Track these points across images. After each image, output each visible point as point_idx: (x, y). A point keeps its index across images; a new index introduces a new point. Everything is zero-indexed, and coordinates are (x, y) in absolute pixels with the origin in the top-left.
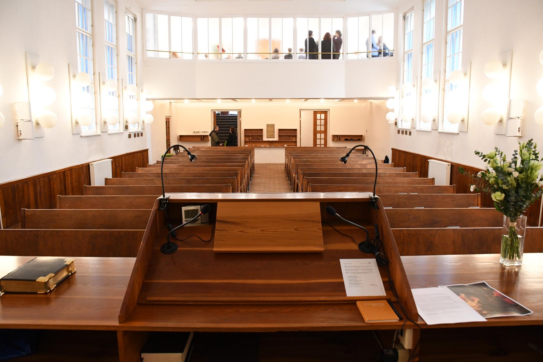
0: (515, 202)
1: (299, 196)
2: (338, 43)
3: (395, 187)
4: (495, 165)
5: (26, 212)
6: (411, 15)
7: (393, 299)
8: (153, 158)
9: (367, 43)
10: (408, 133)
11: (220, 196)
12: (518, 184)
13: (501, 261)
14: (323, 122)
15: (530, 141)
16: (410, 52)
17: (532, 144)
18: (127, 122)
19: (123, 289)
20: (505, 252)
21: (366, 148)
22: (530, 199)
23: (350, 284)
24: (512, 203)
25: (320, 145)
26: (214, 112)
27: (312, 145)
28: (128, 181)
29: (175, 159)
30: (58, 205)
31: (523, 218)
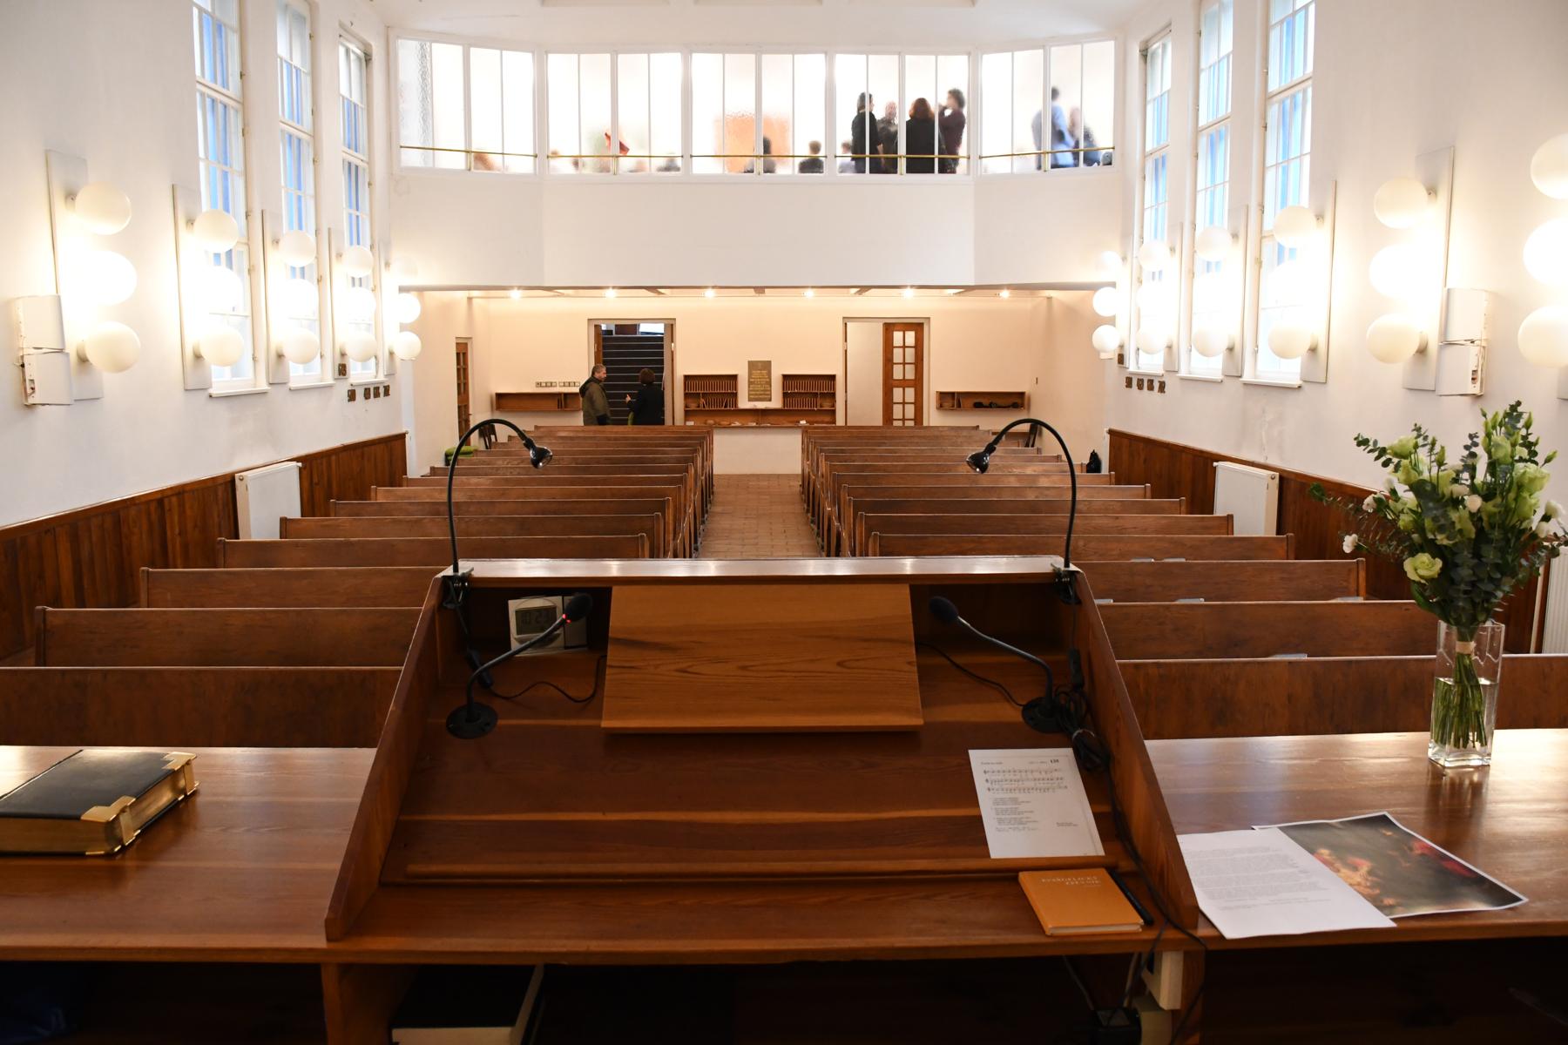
0: (1473, 584)
1: (842, 567)
2: (953, 127)
3: (1119, 540)
4: (1414, 477)
5: (49, 618)
6: (1164, 46)
7: (1126, 865)
8: (419, 461)
9: (1037, 130)
10: (1156, 385)
11: (613, 568)
12: (1480, 531)
13: (1430, 753)
14: (910, 354)
15: (1514, 408)
16: (1163, 152)
17: (1520, 414)
18: (343, 355)
19: (341, 840)
20: (1443, 725)
21: (1037, 426)
22: (1514, 574)
23: (1000, 821)
24: (1463, 587)
25: (904, 420)
26: (597, 327)
27: (880, 423)
28: (346, 525)
29: (484, 463)
30: (143, 596)
31: (1493, 627)
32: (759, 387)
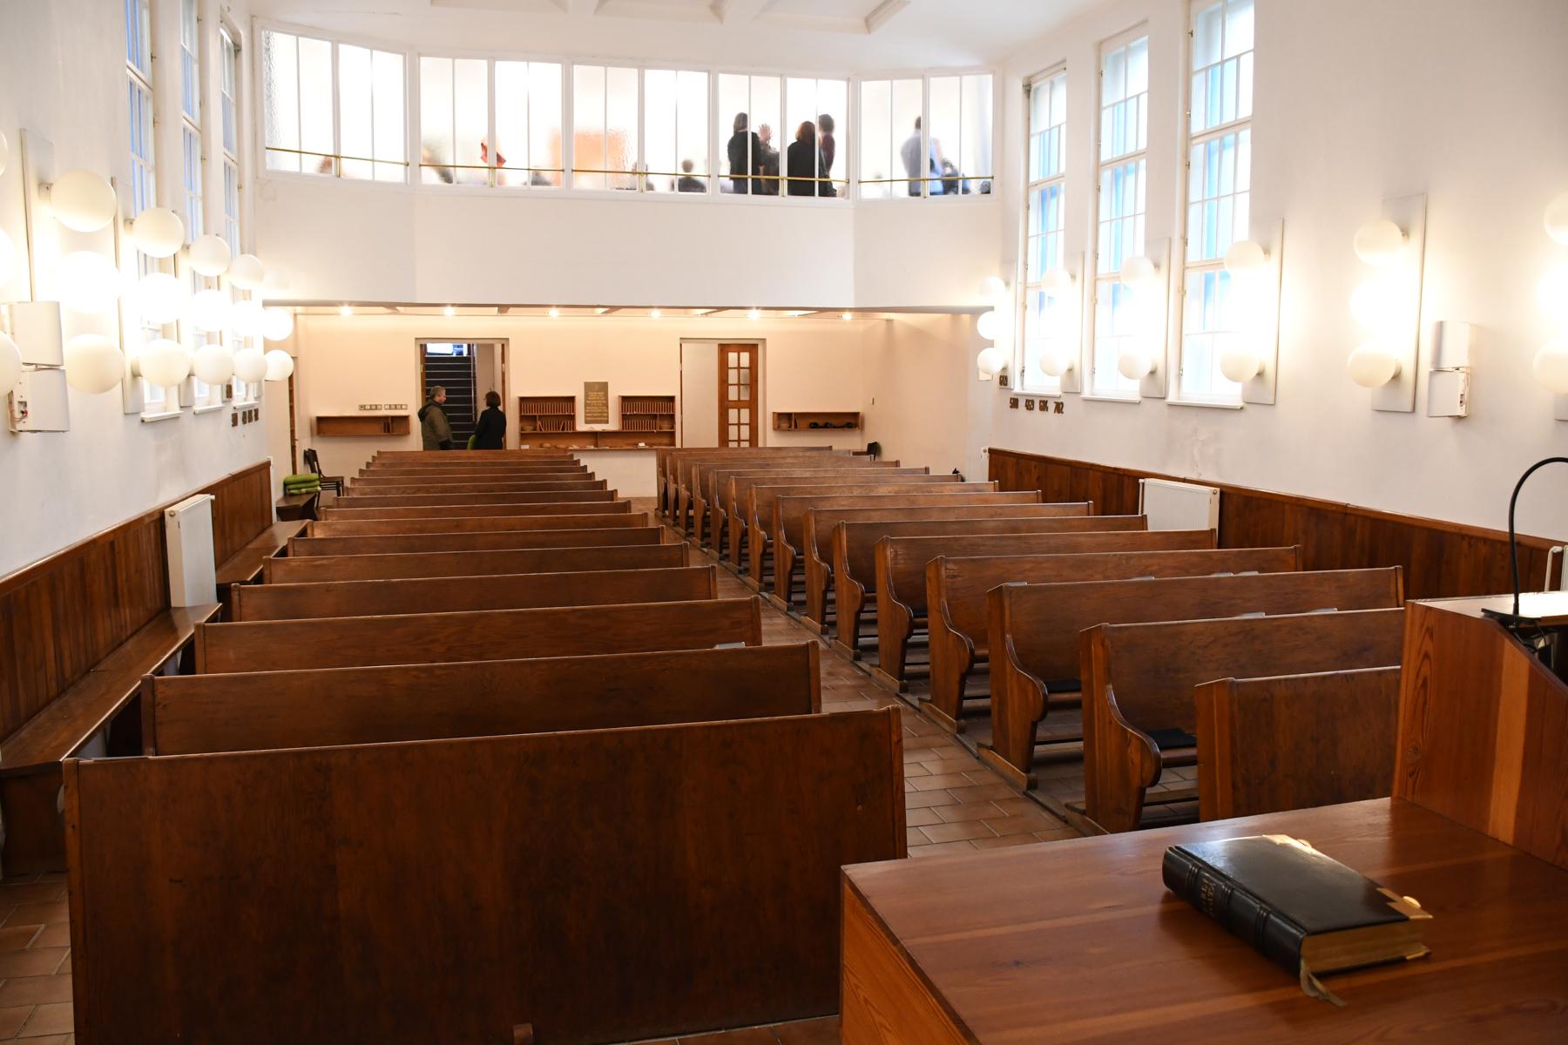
5: (160, 688)
25: (739, 441)
27: (715, 444)
32: (596, 409)
